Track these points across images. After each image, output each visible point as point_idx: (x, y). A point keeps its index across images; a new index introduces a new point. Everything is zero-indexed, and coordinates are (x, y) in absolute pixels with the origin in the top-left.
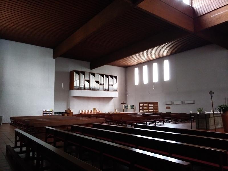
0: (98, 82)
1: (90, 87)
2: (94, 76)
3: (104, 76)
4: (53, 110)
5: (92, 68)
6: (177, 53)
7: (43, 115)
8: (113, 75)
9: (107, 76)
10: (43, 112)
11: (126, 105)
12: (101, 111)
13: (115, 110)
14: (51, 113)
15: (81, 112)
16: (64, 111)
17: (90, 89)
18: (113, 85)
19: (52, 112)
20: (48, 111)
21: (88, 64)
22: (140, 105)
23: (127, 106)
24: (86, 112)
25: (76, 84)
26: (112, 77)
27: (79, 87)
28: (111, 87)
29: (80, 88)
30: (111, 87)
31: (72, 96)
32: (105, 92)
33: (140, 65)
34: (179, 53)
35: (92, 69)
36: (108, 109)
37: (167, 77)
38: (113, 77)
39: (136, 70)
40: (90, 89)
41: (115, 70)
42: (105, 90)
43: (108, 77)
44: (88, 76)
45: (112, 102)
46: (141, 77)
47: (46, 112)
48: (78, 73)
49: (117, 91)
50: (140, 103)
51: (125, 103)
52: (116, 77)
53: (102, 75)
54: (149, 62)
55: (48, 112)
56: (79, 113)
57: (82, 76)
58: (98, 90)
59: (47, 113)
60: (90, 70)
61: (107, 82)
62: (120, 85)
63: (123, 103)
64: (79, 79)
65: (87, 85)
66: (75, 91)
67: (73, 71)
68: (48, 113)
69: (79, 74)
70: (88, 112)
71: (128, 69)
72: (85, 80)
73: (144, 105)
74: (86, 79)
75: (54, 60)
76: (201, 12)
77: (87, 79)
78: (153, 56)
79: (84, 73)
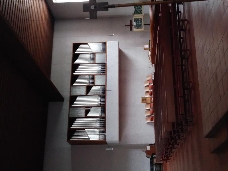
0: (89, 88)
5: (60, 98)
12: (147, 77)
13: (145, 49)
16: (148, 160)
17: (103, 106)
23: (137, 20)
25: (93, 135)
28: (98, 59)
29: (103, 127)
30: (98, 59)
32: (108, 49)
36: (143, 65)
38: (77, 52)
40: (103, 106)
41: (63, 42)
44: (77, 110)
45: (129, 52)
48: (71, 132)
49: (105, 44)
51: (131, 21)
52: (76, 46)
53: (74, 78)
56: (152, 125)
57: (79, 124)
58: (104, 87)
60: (65, 103)
61: (87, 69)
63: (131, 25)
64: (84, 129)
67: (69, 142)
69: (75, 130)
70: (149, 88)
72: (86, 117)
74: (83, 114)
77: (82, 113)
79: (72, 120)
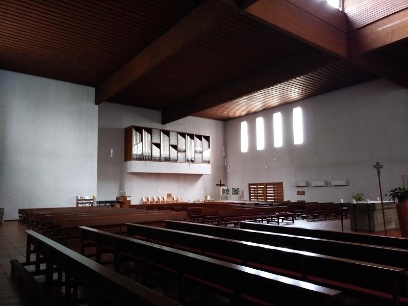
0: (175, 147)
1: (162, 156)
2: (169, 137)
3: (187, 137)
4: (95, 196)
5: (165, 121)
6: (316, 95)
7: (77, 206)
8: (202, 134)
9: (192, 136)
10: (78, 200)
11: (225, 188)
12: (181, 199)
13: (206, 197)
14: (92, 202)
15: (144, 200)
16: (114, 199)
17: (160, 159)
18: (202, 153)
19: (93, 200)
20: (86, 198)
21: (158, 114)
22: (250, 188)
23: (228, 190)
24: (154, 200)
25: (137, 150)
26: (200, 137)
27: (142, 155)
28: (198, 156)
29: (143, 158)
30: (198, 156)
31: (129, 171)
32: (187, 164)
33: (251, 116)
34: (320, 94)
35: (164, 124)
36: (193, 194)
37: (299, 138)
38: (203, 139)
39: (244, 125)
40: (160, 159)
41: (205, 126)
42: (189, 161)
43: (193, 139)
44: (158, 135)
45: (200, 183)
46: (252, 137)
47: (83, 200)
48: (139, 130)
49: (209, 162)
50: (250, 185)
51: (224, 185)
52: (207, 138)
53: (183, 135)
54: (267, 112)
55: (86, 200)
56: (141, 202)
57: (146, 136)
58: (176, 161)
59: (84, 202)
60: (161, 125)
61: (191, 147)
62: (215, 151)
63: (221, 185)
64: (142, 141)
65: (156, 152)
66: (133, 163)
67: (131, 126)
68: (86, 202)
69: (141, 133)
70: (157, 200)
71: (229, 124)
72: (152, 143)
73: (257, 188)
74: (154, 141)
75: (97, 107)
76: (359, 21)
77: (156, 140)
78: (275, 101)
79: (150, 131)
